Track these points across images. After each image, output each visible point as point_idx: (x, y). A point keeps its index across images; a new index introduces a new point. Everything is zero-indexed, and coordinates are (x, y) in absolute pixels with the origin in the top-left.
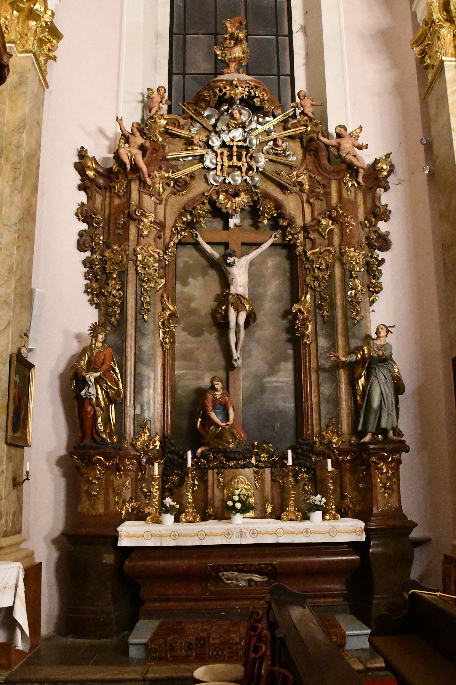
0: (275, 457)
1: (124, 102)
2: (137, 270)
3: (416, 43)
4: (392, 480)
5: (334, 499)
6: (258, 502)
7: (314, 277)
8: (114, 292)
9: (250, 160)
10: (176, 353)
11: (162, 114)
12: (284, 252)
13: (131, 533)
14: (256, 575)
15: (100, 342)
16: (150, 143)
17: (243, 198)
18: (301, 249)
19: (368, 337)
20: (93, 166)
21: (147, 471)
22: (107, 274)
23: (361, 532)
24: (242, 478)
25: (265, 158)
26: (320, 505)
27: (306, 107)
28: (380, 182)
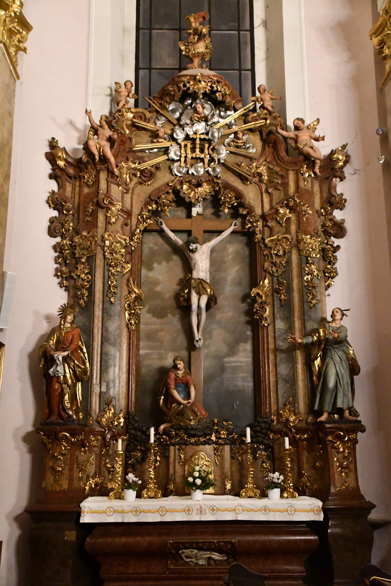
0: (234, 434)
1: (92, 96)
2: (104, 256)
3: (374, 33)
4: (349, 459)
5: (292, 477)
6: (217, 478)
7: (272, 263)
8: (83, 276)
9: (212, 152)
10: (141, 334)
11: (129, 107)
12: (244, 239)
13: (93, 509)
14: (215, 553)
15: (69, 323)
16: (118, 135)
17: (206, 188)
18: (259, 236)
19: (324, 320)
20: (63, 156)
21: (111, 447)
22: (76, 258)
23: (319, 511)
24: (202, 454)
25: (226, 150)
26: (278, 483)
27: (265, 101)
28: (337, 172)
